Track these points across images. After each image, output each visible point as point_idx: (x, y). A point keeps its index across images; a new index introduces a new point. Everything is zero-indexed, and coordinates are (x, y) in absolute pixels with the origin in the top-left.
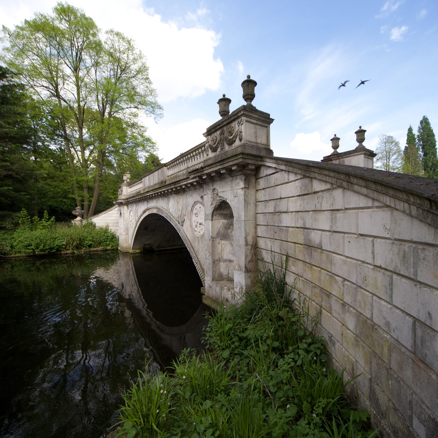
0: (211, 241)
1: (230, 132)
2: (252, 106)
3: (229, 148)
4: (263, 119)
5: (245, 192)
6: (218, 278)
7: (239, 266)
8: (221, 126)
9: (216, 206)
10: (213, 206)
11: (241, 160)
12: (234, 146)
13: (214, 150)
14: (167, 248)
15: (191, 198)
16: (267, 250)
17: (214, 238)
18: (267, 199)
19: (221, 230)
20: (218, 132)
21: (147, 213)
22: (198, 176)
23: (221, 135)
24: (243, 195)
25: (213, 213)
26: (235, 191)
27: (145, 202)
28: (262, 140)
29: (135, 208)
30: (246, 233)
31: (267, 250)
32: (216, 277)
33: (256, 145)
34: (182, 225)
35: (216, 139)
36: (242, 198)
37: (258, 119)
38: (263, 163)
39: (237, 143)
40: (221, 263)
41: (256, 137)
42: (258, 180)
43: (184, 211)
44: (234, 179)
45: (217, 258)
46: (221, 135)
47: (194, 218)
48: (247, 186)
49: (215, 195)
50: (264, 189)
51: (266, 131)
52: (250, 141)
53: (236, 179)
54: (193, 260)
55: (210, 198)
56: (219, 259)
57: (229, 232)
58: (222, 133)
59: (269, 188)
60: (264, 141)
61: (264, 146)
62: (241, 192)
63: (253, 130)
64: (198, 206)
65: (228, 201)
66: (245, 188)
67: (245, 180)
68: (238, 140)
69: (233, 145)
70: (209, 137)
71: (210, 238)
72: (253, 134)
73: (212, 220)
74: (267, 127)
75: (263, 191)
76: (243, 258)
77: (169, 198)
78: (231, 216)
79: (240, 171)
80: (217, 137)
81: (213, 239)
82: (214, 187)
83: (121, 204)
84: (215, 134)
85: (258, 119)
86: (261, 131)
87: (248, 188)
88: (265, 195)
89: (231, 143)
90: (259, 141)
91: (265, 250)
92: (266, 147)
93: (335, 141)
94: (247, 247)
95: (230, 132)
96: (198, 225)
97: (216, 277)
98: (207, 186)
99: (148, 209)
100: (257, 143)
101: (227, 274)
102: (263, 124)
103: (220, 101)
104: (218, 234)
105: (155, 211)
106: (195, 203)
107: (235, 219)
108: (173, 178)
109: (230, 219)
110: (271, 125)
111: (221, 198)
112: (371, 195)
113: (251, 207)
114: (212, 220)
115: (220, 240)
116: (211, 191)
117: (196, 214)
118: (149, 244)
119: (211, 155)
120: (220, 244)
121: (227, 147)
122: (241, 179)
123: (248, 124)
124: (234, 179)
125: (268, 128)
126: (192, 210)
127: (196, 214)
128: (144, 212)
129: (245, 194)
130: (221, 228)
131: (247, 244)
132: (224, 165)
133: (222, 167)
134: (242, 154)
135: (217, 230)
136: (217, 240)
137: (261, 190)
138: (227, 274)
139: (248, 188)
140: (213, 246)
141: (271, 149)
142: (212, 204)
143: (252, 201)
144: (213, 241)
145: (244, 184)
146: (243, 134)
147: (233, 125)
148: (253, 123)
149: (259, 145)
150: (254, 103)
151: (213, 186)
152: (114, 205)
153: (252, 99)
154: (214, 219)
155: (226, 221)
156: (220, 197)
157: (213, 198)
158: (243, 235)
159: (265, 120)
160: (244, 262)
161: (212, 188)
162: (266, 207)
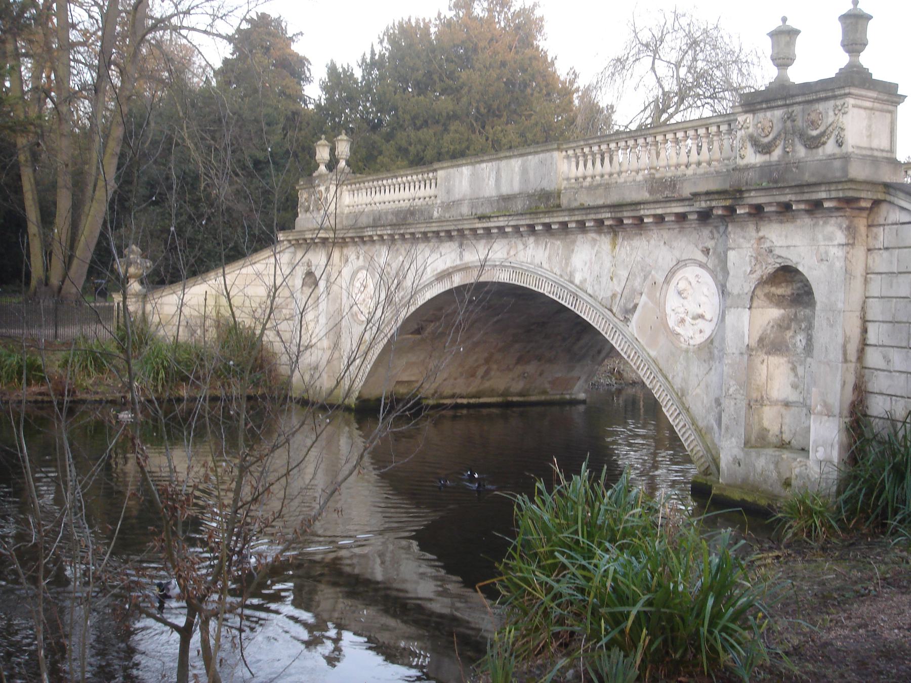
0: (746, 357)
2: (860, 66)
6: (756, 440)
7: (825, 405)
8: (788, 102)
9: (762, 276)
13: (765, 149)
14: (459, 401)
16: (890, 372)
17: (752, 350)
18: (896, 271)
19: (769, 332)
20: (778, 113)
21: (457, 280)
23: (785, 122)
24: (843, 260)
26: (822, 249)
27: (447, 244)
30: (846, 337)
31: (890, 372)
32: (753, 438)
33: (869, 153)
34: (626, 320)
35: (772, 128)
36: (839, 264)
38: (888, 198)
40: (766, 409)
41: (869, 136)
42: (875, 230)
44: (821, 223)
45: (755, 395)
46: (785, 122)
48: (851, 242)
50: (887, 249)
51: (888, 121)
52: (858, 147)
53: (825, 223)
55: (747, 258)
56: (762, 397)
57: (788, 337)
59: (899, 248)
60: (885, 144)
61: (885, 154)
62: (836, 253)
63: (865, 123)
64: (691, 272)
65: (800, 268)
66: (847, 244)
69: (820, 150)
71: (744, 349)
72: (864, 131)
73: (750, 308)
74: (890, 112)
75: (885, 254)
76: (838, 386)
77: (574, 242)
80: (775, 121)
82: (761, 234)
86: (881, 123)
87: (853, 245)
88: (891, 262)
90: (875, 144)
91: (884, 370)
92: (889, 155)
93: (784, 38)
94: (845, 365)
96: (688, 319)
97: (753, 438)
98: (738, 230)
100: (872, 149)
101: (778, 433)
102: (885, 107)
104: (761, 340)
106: (680, 264)
107: (818, 307)
110: (900, 108)
111: (779, 260)
114: (750, 308)
115: (766, 353)
118: (409, 383)
120: (765, 363)
122: (841, 228)
123: (856, 110)
124: (821, 223)
125: (893, 113)
129: (846, 258)
130: (769, 328)
131: (846, 360)
135: (761, 332)
136: (759, 353)
138: (778, 433)
139: (853, 245)
140: (750, 369)
145: (846, 236)
147: (821, 107)
148: (865, 108)
149: (876, 153)
150: (866, 59)
151: (758, 230)
153: (859, 52)
154: (754, 305)
155: (782, 311)
156: (779, 257)
157: (756, 259)
158: (840, 340)
159: (890, 95)
160: (838, 396)
162: (891, 287)
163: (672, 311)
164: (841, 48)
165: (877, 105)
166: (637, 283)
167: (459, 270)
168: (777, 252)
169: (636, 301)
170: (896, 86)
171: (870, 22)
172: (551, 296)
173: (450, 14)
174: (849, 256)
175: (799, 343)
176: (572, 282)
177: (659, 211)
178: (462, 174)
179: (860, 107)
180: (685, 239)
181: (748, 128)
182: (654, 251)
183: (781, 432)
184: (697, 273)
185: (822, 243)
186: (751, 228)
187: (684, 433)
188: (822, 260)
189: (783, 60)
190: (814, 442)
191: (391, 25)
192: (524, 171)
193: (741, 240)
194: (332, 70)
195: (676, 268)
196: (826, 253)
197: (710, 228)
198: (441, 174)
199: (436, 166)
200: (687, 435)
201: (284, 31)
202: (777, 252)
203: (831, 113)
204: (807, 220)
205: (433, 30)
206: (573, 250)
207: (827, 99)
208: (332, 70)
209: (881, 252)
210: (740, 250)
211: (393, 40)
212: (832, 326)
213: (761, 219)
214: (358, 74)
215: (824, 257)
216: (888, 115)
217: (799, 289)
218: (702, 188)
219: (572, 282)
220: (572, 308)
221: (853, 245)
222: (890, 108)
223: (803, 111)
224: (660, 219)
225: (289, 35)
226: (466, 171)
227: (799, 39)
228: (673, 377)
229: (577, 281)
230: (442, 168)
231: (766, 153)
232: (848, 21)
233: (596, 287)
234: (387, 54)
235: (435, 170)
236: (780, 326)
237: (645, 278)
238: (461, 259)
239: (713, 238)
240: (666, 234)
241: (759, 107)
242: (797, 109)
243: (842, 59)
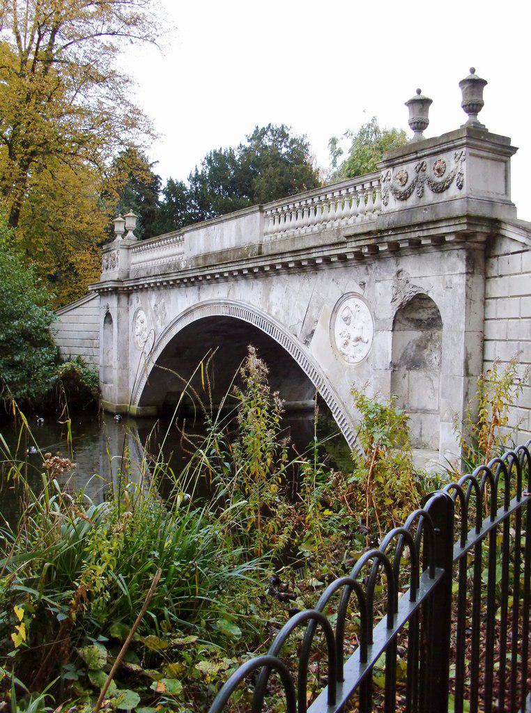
0: (390, 372)
1: (439, 170)
2: (479, 124)
3: (434, 197)
4: (499, 149)
5: (467, 280)
8: (418, 155)
9: (402, 304)
10: (398, 303)
11: (465, 227)
12: (445, 196)
13: (404, 197)
15: (333, 284)
20: (412, 165)
21: (197, 316)
22: (368, 246)
24: (464, 287)
25: (395, 317)
26: (447, 278)
27: (191, 289)
28: (495, 188)
29: (153, 301)
34: (307, 343)
36: (461, 291)
37: (493, 151)
39: (453, 191)
43: (314, 313)
47: (340, 326)
48: (470, 271)
49: (402, 283)
53: (449, 255)
54: (334, 416)
55: (390, 289)
57: (425, 355)
58: (421, 169)
64: (351, 303)
65: (430, 295)
67: (468, 259)
68: (454, 186)
69: (445, 194)
70: (391, 170)
77: (271, 282)
78: (435, 322)
79: (458, 243)
80: (409, 173)
81: (394, 366)
82: (400, 268)
83: (104, 293)
84: (405, 167)
85: (490, 149)
89: (440, 189)
92: (504, 198)
93: (421, 104)
95: (439, 170)
99: (200, 307)
102: (499, 157)
103: (412, 103)
104: (404, 356)
105: (223, 312)
106: (344, 297)
107: (445, 328)
108: (283, 240)
109: (428, 329)
110: (513, 158)
111: (415, 289)
112: (177, 234)
113: (478, 306)
114: (393, 331)
116: (394, 274)
117: (346, 319)
119: (394, 205)
121: (430, 196)
123: (473, 159)
125: (507, 163)
126: (335, 311)
127: (346, 319)
128: (188, 312)
129: (467, 285)
132: (431, 231)
133: (426, 233)
134: (468, 216)
135: (402, 351)
137: (496, 277)
141: (513, 200)
142: (394, 300)
143: (478, 295)
144: (394, 371)
145: (467, 266)
146: (465, 177)
147: (443, 157)
150: (482, 117)
152: (87, 293)
154: (397, 328)
156: (414, 286)
158: (462, 357)
161: (395, 269)
163: (339, 336)
164: (462, 109)
165: (491, 155)
166: (314, 313)
167: (198, 308)
168: (412, 282)
169: (313, 328)
170: (508, 140)
171: (486, 88)
172: (256, 325)
173: (248, 145)
174: (469, 283)
175: (434, 360)
176: (270, 315)
177: (326, 254)
178: (199, 235)
179: (478, 156)
180: (347, 276)
181: (389, 180)
182: (327, 286)
183: (421, 436)
184: (357, 303)
185: (447, 273)
186: (392, 262)
187: (349, 435)
188: (447, 287)
189: (420, 125)
190: (443, 444)
191: (209, 153)
192: (239, 230)
193: (385, 274)
194: (171, 182)
195: (341, 300)
196: (451, 281)
197: (365, 266)
198: (186, 235)
199: (183, 230)
200: (350, 437)
201: (147, 161)
202: (412, 282)
203: (453, 161)
204: (436, 254)
205: (236, 153)
206: (270, 289)
207: (449, 149)
208: (171, 182)
209: (496, 279)
210: (384, 282)
211: (210, 161)
212: (455, 345)
213: (400, 256)
214: (188, 185)
215: (449, 285)
216: (503, 164)
217: (433, 314)
218: (359, 231)
219: (270, 315)
220: (270, 335)
221: (472, 273)
222: (504, 158)
223: (431, 162)
224: (327, 260)
225: (150, 162)
226: (202, 232)
227: (431, 108)
228: (340, 389)
229: (273, 314)
230: (187, 232)
231: (403, 200)
232: (466, 86)
233: (286, 317)
234: (208, 172)
235: (183, 234)
236: (418, 346)
237: (320, 309)
238: (199, 299)
239: (368, 274)
240: (334, 274)
241: (397, 162)
242: (426, 160)
243: (463, 118)
